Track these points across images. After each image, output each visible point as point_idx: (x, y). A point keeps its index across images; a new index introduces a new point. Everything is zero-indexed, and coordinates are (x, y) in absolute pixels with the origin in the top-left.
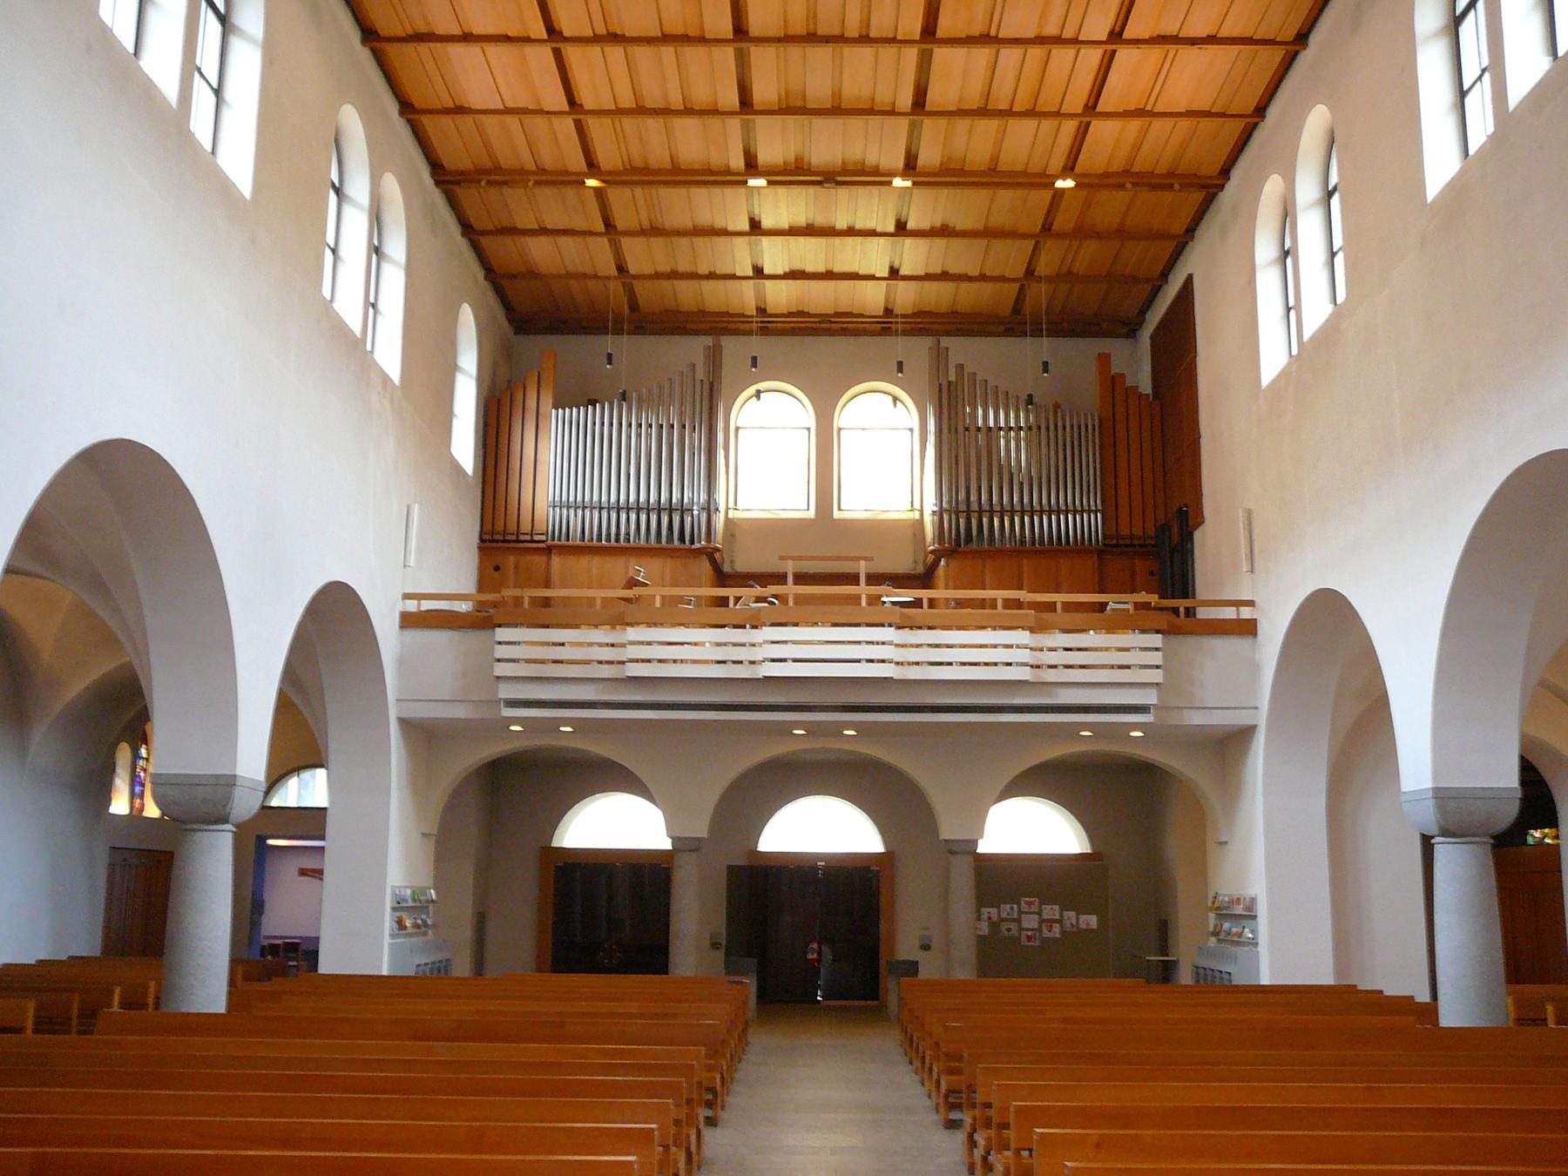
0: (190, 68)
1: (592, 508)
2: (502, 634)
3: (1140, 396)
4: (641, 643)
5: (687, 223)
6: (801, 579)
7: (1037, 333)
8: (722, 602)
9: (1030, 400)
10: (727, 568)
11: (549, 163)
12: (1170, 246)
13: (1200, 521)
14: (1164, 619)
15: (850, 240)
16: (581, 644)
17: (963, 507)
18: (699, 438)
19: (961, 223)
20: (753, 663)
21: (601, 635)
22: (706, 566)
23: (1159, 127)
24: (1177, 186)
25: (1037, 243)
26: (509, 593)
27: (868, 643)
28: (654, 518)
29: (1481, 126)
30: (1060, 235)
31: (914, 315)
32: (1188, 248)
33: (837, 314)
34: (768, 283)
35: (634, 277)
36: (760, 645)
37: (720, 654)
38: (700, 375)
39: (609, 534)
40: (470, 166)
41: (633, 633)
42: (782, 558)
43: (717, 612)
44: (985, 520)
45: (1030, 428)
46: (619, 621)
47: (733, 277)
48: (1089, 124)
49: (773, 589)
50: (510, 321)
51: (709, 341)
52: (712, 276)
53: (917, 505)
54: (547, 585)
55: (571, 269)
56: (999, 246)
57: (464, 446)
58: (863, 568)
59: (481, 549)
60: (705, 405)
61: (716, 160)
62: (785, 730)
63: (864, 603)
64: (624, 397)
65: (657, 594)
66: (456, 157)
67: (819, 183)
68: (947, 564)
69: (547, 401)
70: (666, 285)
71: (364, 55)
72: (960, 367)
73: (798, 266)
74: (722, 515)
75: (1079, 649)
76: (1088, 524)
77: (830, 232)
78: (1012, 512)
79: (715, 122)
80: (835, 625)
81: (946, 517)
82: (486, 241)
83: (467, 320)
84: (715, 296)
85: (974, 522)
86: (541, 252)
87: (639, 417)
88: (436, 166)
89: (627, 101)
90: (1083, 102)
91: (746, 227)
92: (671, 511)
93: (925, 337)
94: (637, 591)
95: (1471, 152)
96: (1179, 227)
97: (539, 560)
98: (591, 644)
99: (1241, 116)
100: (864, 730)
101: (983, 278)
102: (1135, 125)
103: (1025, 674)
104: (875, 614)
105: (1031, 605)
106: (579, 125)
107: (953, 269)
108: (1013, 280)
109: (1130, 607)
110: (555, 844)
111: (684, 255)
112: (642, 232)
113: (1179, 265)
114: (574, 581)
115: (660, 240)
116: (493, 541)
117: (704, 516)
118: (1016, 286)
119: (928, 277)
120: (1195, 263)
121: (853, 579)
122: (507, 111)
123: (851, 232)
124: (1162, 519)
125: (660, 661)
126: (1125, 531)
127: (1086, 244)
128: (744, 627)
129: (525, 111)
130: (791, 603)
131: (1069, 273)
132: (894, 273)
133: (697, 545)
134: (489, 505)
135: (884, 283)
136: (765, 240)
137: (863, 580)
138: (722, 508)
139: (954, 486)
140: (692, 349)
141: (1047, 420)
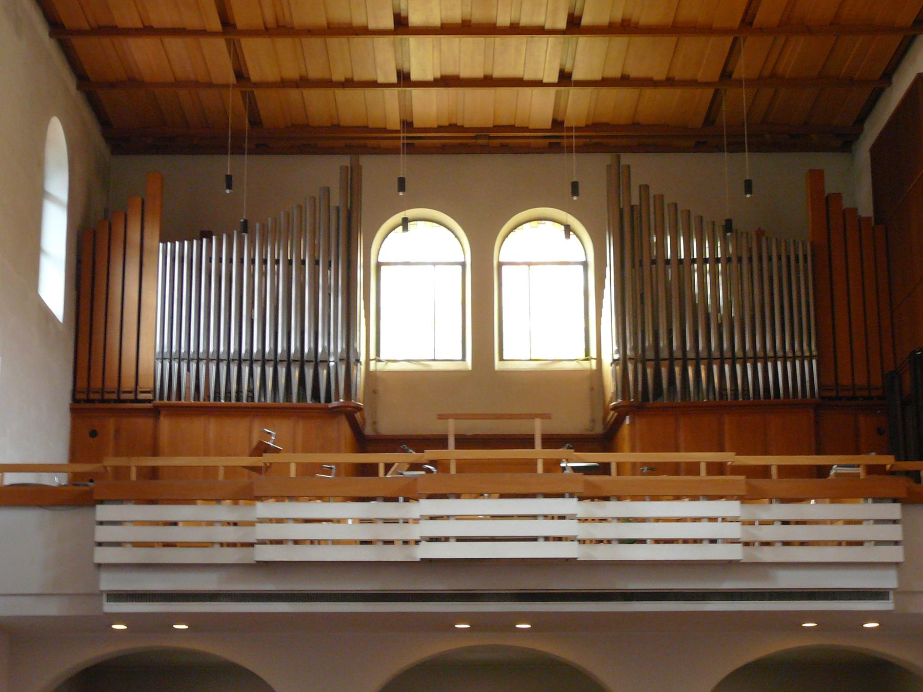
1: (208, 360)
2: (104, 512)
3: (860, 220)
4: (271, 521)
6: (463, 442)
7: (736, 146)
8: (369, 470)
9: (728, 226)
10: (368, 431)
14: (901, 485)
15: (514, 40)
16: (198, 523)
17: (650, 354)
18: (334, 277)
19: (646, 18)
20: (406, 542)
21: (224, 511)
22: (345, 428)
25: (735, 40)
26: (111, 462)
27: (546, 517)
28: (282, 371)
30: (761, 30)
31: (587, 127)
33: (497, 128)
34: (416, 92)
35: (256, 85)
36: (416, 521)
37: (366, 532)
38: (336, 200)
39: (228, 392)
41: (264, 509)
42: (441, 417)
43: (361, 484)
44: (677, 370)
45: (729, 260)
46: (251, 496)
47: (374, 84)
49: (431, 454)
51: (345, 160)
52: (349, 83)
53: (593, 354)
54: (155, 451)
56: (692, 45)
57: (53, 288)
58: (538, 428)
59: (73, 410)
60: (342, 240)
62: (445, 623)
64: (245, 227)
65: (293, 461)
68: (632, 423)
70: (294, 94)
72: (645, 188)
73: (450, 70)
74: (363, 367)
75: (798, 523)
76: (797, 371)
77: (490, 29)
78: (710, 361)
80: (502, 496)
81: (630, 367)
82: (78, 43)
83: (57, 138)
84: (353, 107)
85: (664, 371)
86: (144, 55)
91: (389, 23)
92: (302, 363)
93: (599, 156)
94: (267, 458)
97: (144, 424)
98: (211, 523)
100: (540, 623)
101: (670, 82)
103: (735, 553)
104: (553, 482)
105: (737, 470)
107: (634, 72)
108: (707, 84)
109: (860, 471)
111: (316, 59)
113: (905, 64)
114: (187, 449)
115: (288, 41)
116: (103, 401)
118: (709, 93)
119: (605, 82)
121: (526, 441)
123: (515, 29)
125: (296, 542)
128: (396, 500)
130: (453, 470)
132: (565, 78)
133: (334, 404)
134: (84, 356)
135: (552, 91)
136: (413, 40)
137: (538, 442)
138: (363, 359)
139: (639, 332)
140: (326, 171)
141: (750, 250)
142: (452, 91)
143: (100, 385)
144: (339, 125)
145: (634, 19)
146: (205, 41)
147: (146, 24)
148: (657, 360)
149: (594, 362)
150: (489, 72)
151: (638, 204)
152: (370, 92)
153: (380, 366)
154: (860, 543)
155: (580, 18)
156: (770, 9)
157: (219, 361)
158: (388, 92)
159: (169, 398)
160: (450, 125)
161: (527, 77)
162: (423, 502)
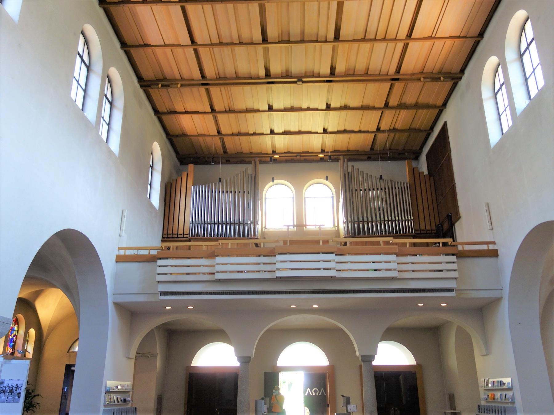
0: (99, 116)
1: (208, 224)
5: (243, 107)
11: (186, 75)
12: (424, 134)
13: (458, 217)
17: (356, 220)
19: (352, 104)
23: (439, 44)
24: (442, 79)
29: (507, 122)
30: (384, 131)
32: (444, 112)
33: (303, 152)
34: (276, 137)
35: (224, 135)
40: (154, 78)
47: (262, 134)
48: (408, 44)
50: (178, 158)
52: (254, 134)
55: (200, 132)
57: (156, 199)
60: (251, 189)
61: (253, 72)
63: (321, 243)
66: (148, 74)
67: (295, 82)
69: (190, 182)
71: (121, 53)
73: (287, 129)
79: (251, 47)
83: (157, 148)
85: (361, 226)
87: (226, 188)
88: (140, 79)
89: (215, 40)
90: (406, 34)
95: (532, 98)
96: (440, 103)
99: (425, 131)
101: (360, 132)
102: (428, 43)
106: (196, 51)
110: (192, 365)
112: (226, 112)
117: (253, 226)
118: (373, 135)
120: (448, 116)
122: (165, 45)
123: (308, 109)
124: (438, 223)
126: (423, 227)
127: (402, 111)
129: (173, 45)
131: (394, 129)
132: (325, 131)
139: (352, 211)
142: (288, 136)
143: (171, 232)
145: (348, 105)
150: (300, 129)
152: (261, 137)
153: (266, 230)
154: (441, 271)
156: (393, 102)
157: (211, 224)
161: (313, 131)
162: (278, 256)
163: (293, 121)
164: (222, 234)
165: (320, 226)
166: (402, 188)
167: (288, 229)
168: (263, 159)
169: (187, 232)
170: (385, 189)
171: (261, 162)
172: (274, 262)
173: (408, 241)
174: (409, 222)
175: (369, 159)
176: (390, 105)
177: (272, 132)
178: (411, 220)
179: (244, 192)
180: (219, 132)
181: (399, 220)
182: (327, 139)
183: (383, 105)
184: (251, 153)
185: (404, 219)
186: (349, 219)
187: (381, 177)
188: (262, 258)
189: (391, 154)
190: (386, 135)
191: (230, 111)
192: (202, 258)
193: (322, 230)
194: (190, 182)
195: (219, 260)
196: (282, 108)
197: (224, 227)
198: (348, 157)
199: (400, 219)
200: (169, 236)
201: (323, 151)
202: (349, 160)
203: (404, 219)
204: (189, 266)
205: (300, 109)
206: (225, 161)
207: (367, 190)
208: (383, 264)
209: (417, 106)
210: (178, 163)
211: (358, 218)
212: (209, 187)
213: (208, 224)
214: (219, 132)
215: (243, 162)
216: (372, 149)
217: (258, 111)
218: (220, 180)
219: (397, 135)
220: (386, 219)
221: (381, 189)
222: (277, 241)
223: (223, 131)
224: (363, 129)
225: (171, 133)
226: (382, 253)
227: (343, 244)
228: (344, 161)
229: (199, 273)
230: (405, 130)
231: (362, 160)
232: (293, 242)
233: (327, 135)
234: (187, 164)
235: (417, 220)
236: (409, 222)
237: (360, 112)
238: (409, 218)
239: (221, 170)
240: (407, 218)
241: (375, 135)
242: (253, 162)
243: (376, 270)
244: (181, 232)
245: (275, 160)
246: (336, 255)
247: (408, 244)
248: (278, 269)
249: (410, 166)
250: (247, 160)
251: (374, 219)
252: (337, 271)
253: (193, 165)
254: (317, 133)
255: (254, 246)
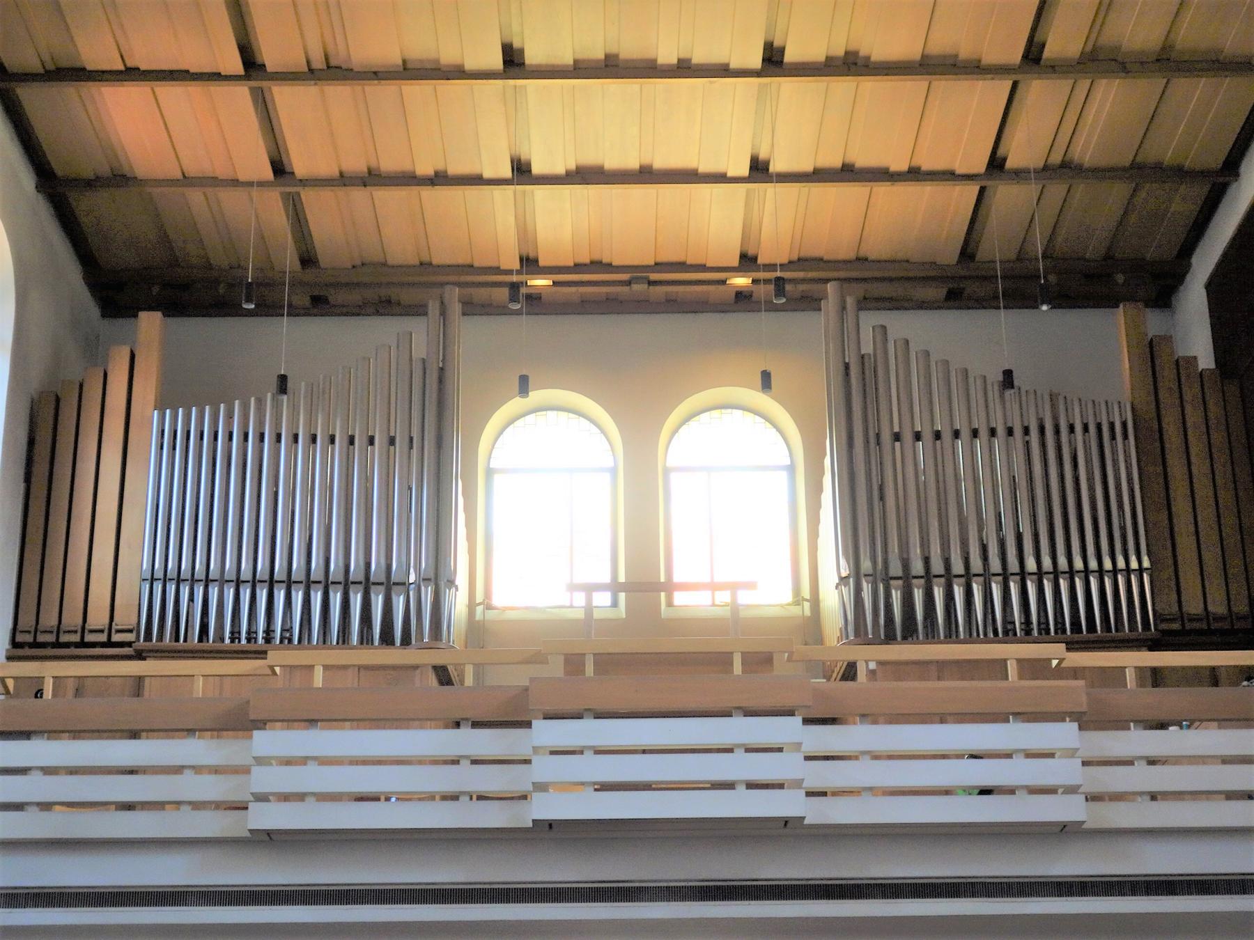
1: (222, 582)
5: (387, 52)
17: (896, 569)
19: (880, 48)
28: (336, 600)
30: (1019, 175)
33: (659, 266)
34: (540, 193)
35: (304, 183)
47: (477, 180)
52: (440, 179)
55: (192, 169)
60: (431, 431)
69: (146, 391)
73: (590, 157)
85: (918, 595)
87: (311, 422)
91: (497, 62)
101: (914, 174)
118: (972, 190)
119: (818, 175)
123: (684, 69)
127: (1102, 84)
132: (759, 170)
143: (54, 622)
144: (430, 264)
146: (217, 89)
147: (129, 65)
148: (907, 578)
149: (807, 605)
150: (646, 160)
151: (871, 352)
152: (472, 192)
153: (490, 615)
155: (782, 51)
156: (1063, 41)
157: (238, 583)
158: (498, 192)
159: (161, 636)
160: (592, 262)
161: (703, 168)
163: (614, 123)
164: (287, 629)
165: (734, 587)
166: (1099, 427)
167: (589, 609)
168: (481, 294)
169: (125, 617)
170: (1026, 431)
171: (471, 308)
172: (523, 752)
173: (1133, 660)
174: (1131, 580)
175: (956, 298)
176: (1047, 54)
177: (522, 171)
178: (1141, 570)
179: (392, 441)
180: (280, 169)
181: (1087, 571)
182: (769, 206)
183: (1016, 56)
184: (425, 265)
185: (1108, 565)
186: (866, 565)
187: (1008, 379)
188: (466, 732)
189: (1052, 278)
190: (1030, 190)
191: (330, 71)
192: (190, 732)
193: (743, 614)
194: (146, 391)
195: (266, 742)
196: (567, 59)
197: (298, 598)
198: (860, 290)
199: (1093, 564)
200: (42, 638)
201: (748, 261)
202: (866, 303)
203: (1108, 565)
204: (132, 771)
205: (648, 69)
206: (306, 301)
207: (947, 436)
208: (1019, 762)
209: (1168, 62)
210: (92, 309)
211: (906, 565)
212: (230, 416)
213: (222, 582)
214: (280, 169)
215: (385, 306)
216: (967, 253)
217: (458, 73)
218: (283, 384)
219: (1081, 190)
220: (1031, 565)
221: (1010, 432)
222: (537, 659)
223: (300, 165)
224: (926, 166)
225: (59, 172)
226: (1017, 715)
227: (839, 669)
228: (837, 307)
229: (178, 804)
230: (1112, 169)
231: (922, 305)
232: (608, 663)
233: (770, 190)
234: (131, 311)
235: (1167, 569)
236: (1131, 580)
237: (913, 87)
238: (1134, 565)
239: (289, 340)
240: (1121, 564)
241: (982, 190)
242: (433, 308)
243: (985, 791)
244: (98, 618)
245: (535, 302)
246: (807, 721)
247: (1130, 676)
248: (541, 787)
249: (1134, 328)
250: (406, 296)
251: (976, 565)
252: (810, 794)
253: (158, 315)
254: (721, 178)
255: (432, 680)
